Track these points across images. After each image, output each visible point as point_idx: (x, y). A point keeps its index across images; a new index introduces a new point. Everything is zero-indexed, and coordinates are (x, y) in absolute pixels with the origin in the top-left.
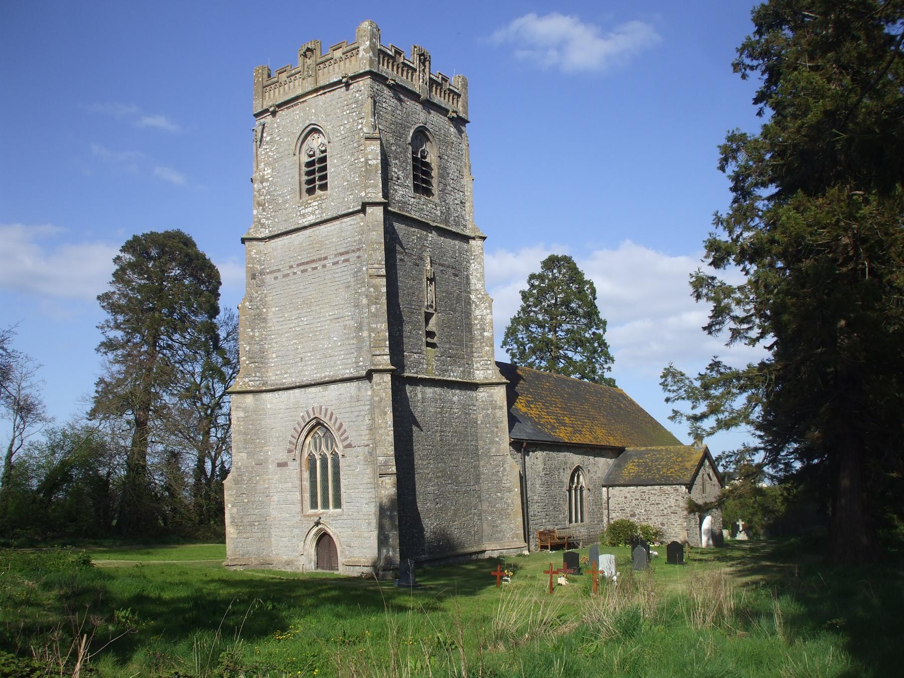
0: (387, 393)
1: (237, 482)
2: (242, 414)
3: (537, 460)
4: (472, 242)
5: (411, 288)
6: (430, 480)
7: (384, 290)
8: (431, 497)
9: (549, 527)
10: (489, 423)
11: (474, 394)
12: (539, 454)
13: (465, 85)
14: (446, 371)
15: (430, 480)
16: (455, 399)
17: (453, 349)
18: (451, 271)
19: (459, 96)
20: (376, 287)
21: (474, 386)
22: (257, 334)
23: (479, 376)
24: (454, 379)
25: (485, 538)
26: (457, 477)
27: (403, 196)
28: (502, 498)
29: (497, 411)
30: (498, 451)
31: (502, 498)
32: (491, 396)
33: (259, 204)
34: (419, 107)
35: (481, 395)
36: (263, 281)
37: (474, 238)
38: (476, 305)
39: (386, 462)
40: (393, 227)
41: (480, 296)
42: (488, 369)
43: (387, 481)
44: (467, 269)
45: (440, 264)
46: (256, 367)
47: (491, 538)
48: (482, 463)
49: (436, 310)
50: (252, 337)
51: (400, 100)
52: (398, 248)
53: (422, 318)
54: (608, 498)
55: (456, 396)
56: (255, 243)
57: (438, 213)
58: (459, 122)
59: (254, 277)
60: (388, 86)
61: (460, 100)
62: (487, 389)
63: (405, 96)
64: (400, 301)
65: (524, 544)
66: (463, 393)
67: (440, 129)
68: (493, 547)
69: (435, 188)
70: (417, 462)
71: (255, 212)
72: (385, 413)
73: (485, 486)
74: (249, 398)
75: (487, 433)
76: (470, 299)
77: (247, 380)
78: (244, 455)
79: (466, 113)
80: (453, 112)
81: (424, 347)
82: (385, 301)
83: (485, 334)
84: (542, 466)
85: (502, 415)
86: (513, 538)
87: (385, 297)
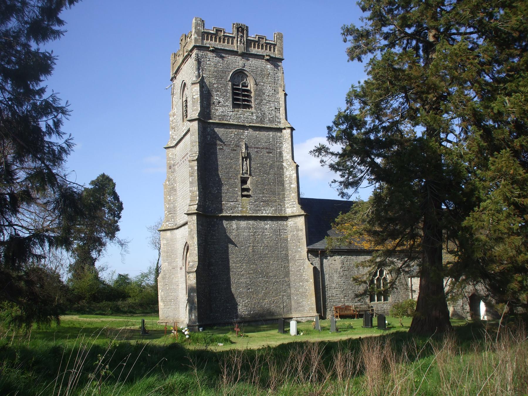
0: (194, 226)
1: (163, 278)
2: (165, 242)
4: (284, 131)
5: (229, 164)
6: (243, 275)
7: (196, 168)
8: (244, 285)
9: (346, 304)
10: (295, 240)
11: (285, 223)
12: (337, 258)
13: (280, 37)
14: (259, 210)
15: (243, 275)
17: (266, 197)
18: (265, 151)
19: (275, 45)
21: (286, 218)
22: (172, 198)
23: (289, 211)
24: (266, 215)
25: (293, 310)
26: (268, 273)
27: (222, 112)
28: (303, 286)
29: (299, 232)
30: (300, 256)
32: (296, 223)
33: (172, 128)
34: (239, 58)
35: (290, 223)
36: (174, 169)
37: (285, 129)
38: (287, 169)
39: (193, 265)
40: (214, 131)
41: (289, 163)
42: (294, 207)
44: (280, 148)
45: (255, 148)
46: (172, 216)
48: (290, 265)
50: (170, 200)
51: (222, 57)
52: (218, 142)
53: (238, 181)
54: (412, 285)
55: (268, 225)
56: (171, 149)
57: (255, 118)
58: (275, 61)
59: (170, 168)
60: (211, 51)
61: (276, 48)
62: (293, 219)
63: (226, 54)
64: (219, 173)
66: (275, 223)
67: (257, 68)
70: (232, 264)
71: (171, 133)
72: (193, 238)
73: (292, 278)
74: (169, 233)
75: (294, 246)
76: (283, 165)
77: (167, 223)
78: (166, 264)
79: (282, 54)
80: (267, 56)
81: (239, 198)
82: (196, 174)
83: (292, 186)
86: (309, 310)
87: (196, 172)
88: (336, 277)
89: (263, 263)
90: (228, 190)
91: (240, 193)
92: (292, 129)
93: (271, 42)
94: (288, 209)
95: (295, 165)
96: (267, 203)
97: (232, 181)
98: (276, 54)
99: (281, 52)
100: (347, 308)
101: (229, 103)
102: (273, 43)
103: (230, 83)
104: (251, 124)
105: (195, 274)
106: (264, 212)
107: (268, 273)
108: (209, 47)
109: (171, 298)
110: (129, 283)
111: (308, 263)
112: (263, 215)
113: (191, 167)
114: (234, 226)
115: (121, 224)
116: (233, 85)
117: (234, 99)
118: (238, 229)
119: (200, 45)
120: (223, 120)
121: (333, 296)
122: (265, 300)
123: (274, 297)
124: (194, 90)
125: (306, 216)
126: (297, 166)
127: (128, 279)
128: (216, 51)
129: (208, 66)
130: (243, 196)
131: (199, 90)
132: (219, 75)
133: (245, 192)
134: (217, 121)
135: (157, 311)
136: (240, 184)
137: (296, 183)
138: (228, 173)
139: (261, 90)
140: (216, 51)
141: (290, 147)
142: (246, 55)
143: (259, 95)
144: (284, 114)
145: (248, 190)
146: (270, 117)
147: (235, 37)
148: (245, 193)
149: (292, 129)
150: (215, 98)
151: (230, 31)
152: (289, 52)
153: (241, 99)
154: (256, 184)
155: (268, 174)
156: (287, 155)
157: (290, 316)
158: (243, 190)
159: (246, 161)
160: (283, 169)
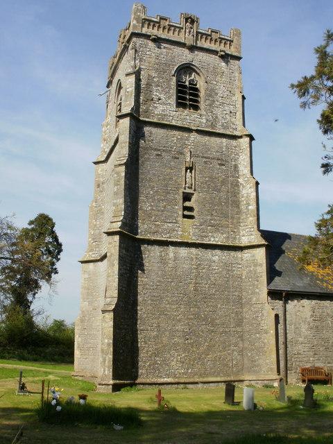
3: (300, 310)
4: (241, 140)
6: (179, 321)
7: (123, 174)
9: (317, 365)
13: (238, 34)
15: (179, 321)
16: (216, 258)
17: (215, 220)
20: (118, 173)
22: (98, 223)
24: (214, 243)
30: (258, 300)
31: (260, 338)
37: (241, 137)
41: (246, 179)
43: (107, 316)
45: (203, 157)
47: (250, 371)
49: (195, 190)
50: (95, 225)
53: (180, 198)
55: (217, 255)
59: (99, 186)
65: (275, 376)
68: (250, 378)
69: (202, 105)
75: (250, 286)
76: (238, 182)
77: (91, 253)
79: (239, 52)
81: (180, 219)
83: (250, 207)
84: (310, 314)
85: (262, 270)
88: (304, 329)
89: (208, 306)
90: (165, 207)
91: (181, 213)
92: (251, 138)
93: (226, 38)
94: (243, 238)
95: (254, 181)
96: (217, 228)
97: (170, 197)
98: (232, 51)
99: (238, 48)
100: (317, 370)
101: (173, 101)
102: (229, 38)
103: (175, 78)
104: (199, 128)
105: (112, 314)
106: (212, 239)
107: (213, 320)
108: (150, 36)
109: (89, 345)
110: (64, 330)
111: (268, 307)
112: (211, 242)
113: (118, 173)
114: (171, 255)
115: (58, 265)
116: (178, 81)
117: (178, 98)
118: (176, 259)
119: (140, 32)
120: (163, 120)
121: (300, 354)
122: (208, 355)
123: (220, 351)
124: (128, 82)
125: (267, 247)
126: (257, 184)
127: (63, 326)
128: (157, 41)
129: (148, 56)
130: (185, 216)
131: (134, 82)
132: (161, 68)
133: (188, 213)
134: (155, 120)
135: (72, 362)
136: (181, 201)
137: (255, 204)
138: (166, 186)
139: (213, 90)
140: (157, 41)
141: (248, 159)
142: (192, 48)
143: (210, 96)
144: (241, 120)
145: (191, 209)
146: (224, 121)
147: (183, 28)
148: (186, 213)
149: (251, 138)
150: (155, 93)
151: (177, 20)
152: (246, 47)
153: (187, 97)
154: (202, 203)
155: (219, 191)
156: (244, 169)
157: (241, 379)
158: (185, 208)
159: (191, 172)
160: (238, 186)
